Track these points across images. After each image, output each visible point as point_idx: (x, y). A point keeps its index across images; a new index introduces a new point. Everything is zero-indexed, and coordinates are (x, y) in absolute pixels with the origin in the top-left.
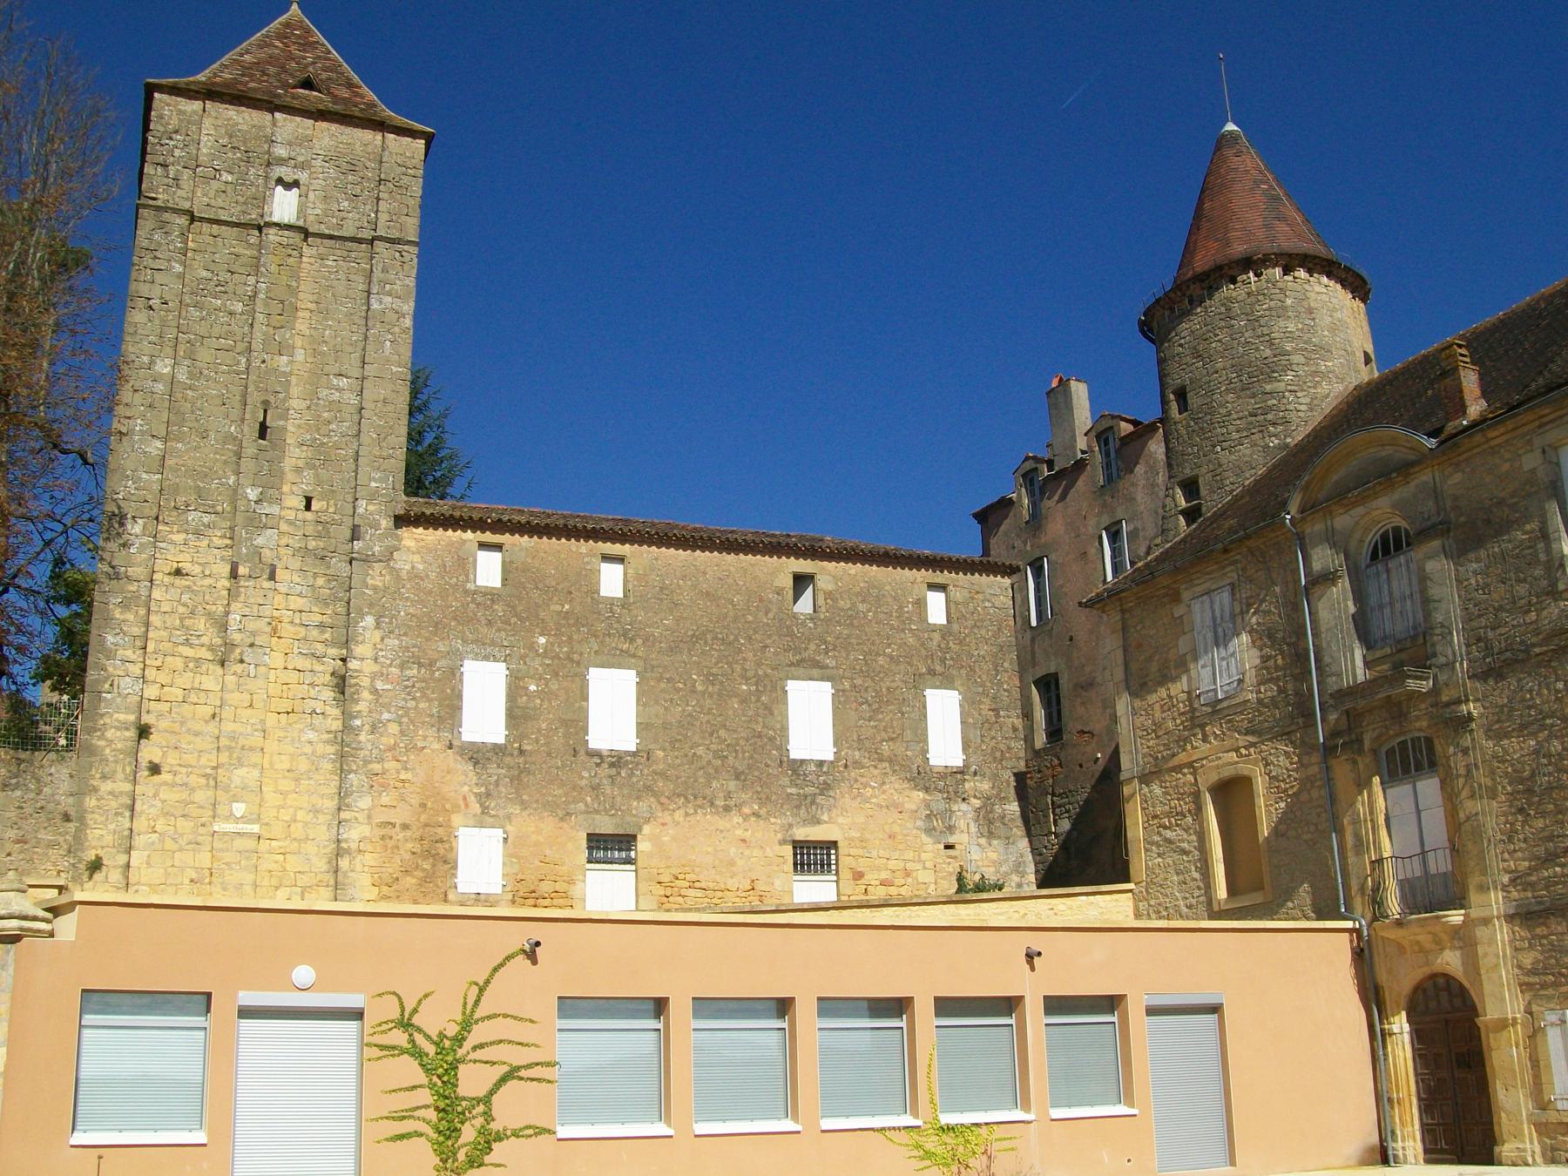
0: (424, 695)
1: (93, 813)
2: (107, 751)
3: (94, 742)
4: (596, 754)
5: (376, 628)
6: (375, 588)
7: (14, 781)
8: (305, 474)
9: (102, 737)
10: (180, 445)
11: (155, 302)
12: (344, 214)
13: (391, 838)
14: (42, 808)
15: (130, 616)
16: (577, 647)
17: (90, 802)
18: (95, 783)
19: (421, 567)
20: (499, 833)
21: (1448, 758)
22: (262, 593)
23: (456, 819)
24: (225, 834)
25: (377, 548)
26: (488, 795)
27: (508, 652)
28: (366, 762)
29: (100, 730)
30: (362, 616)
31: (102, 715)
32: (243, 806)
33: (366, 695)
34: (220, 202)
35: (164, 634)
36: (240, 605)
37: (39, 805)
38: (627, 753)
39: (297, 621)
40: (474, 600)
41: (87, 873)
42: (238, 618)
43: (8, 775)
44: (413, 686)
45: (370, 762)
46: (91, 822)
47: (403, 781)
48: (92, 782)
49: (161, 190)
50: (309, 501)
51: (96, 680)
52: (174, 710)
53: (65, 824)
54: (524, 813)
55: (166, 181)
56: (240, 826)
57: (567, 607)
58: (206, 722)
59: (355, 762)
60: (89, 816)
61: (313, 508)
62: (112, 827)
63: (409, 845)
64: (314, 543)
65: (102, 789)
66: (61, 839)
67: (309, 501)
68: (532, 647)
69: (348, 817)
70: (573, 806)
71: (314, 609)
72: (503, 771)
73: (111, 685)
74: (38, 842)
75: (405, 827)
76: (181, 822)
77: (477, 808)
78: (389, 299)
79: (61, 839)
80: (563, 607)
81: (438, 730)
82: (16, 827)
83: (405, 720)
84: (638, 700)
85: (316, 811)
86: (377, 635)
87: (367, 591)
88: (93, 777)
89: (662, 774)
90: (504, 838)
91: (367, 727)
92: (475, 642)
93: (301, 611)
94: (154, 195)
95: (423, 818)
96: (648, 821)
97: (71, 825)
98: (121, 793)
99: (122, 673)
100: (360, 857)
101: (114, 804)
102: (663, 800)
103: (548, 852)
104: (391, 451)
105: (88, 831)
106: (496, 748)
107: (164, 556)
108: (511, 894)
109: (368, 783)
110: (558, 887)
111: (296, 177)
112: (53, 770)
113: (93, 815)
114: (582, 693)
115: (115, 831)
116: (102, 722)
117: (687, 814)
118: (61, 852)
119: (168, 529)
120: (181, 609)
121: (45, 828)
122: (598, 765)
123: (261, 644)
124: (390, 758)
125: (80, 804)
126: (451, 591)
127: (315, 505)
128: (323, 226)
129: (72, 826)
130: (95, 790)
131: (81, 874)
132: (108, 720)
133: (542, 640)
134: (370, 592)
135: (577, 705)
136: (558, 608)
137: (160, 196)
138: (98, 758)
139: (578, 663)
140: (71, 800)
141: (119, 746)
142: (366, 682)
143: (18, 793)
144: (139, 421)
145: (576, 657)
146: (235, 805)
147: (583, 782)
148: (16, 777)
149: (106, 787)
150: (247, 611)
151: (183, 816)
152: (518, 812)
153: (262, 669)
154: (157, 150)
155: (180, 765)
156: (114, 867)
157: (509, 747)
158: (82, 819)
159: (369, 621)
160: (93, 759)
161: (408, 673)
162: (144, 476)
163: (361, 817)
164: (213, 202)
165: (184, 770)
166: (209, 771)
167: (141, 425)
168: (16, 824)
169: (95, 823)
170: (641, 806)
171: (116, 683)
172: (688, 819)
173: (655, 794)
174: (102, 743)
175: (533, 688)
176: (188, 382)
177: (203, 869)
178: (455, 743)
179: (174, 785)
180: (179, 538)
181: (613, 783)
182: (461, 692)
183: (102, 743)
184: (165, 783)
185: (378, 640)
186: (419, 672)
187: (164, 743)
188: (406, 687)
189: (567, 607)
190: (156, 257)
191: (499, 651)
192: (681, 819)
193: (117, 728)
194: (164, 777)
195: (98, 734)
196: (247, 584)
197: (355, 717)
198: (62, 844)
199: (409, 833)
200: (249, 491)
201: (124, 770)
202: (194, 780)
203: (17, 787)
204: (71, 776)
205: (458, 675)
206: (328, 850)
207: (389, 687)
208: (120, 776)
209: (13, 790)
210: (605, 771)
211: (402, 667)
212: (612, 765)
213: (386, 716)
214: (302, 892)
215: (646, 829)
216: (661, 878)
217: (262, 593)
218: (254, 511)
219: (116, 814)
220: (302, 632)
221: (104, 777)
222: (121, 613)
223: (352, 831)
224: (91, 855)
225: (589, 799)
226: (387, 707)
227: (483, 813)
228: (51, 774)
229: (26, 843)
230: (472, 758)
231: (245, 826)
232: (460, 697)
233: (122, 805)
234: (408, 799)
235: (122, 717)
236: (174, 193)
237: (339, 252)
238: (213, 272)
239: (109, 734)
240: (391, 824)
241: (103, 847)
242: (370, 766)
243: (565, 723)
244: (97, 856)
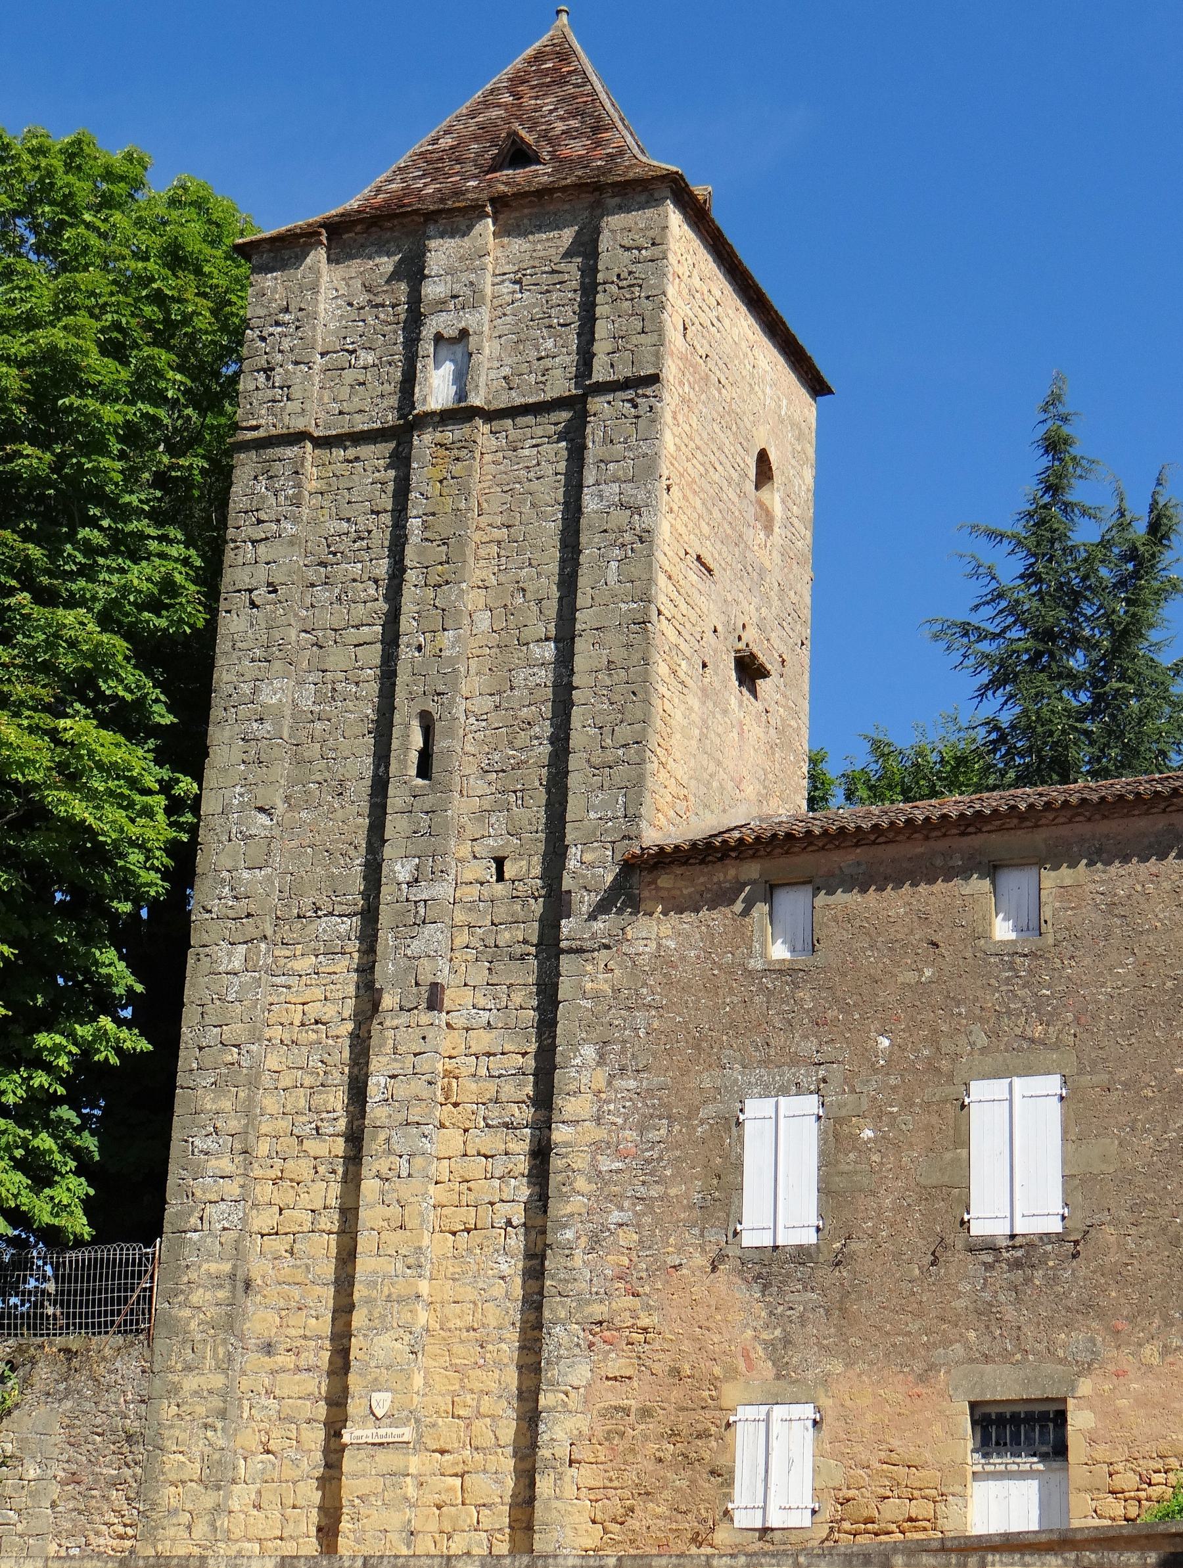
0: (678, 1173)
1: (171, 1427)
2: (193, 1325)
3: (174, 1312)
4: (989, 1246)
5: (599, 1064)
6: (597, 997)
7: (62, 1386)
8: (493, 820)
9: (186, 1304)
10: (304, 814)
11: (260, 594)
12: (548, 363)
13: (622, 1435)
15: (226, 1104)
16: (947, 1046)
19: (672, 944)
20: (808, 1411)
21: (158, 1556)
22: (419, 1032)
23: (730, 1393)
26: (787, 1341)
27: (821, 1073)
28: (582, 1302)
29: (182, 1292)
30: (575, 1047)
32: (388, 1396)
33: (581, 1183)
34: (356, 403)
35: (284, 1124)
36: (385, 1060)
38: (1046, 1237)
39: (484, 1072)
40: (763, 989)
42: (382, 1080)
44: (661, 1159)
45: (588, 1302)
49: (263, 412)
50: (500, 862)
54: (850, 1373)
55: (269, 394)
57: (928, 973)
59: (563, 1304)
61: (507, 876)
63: (652, 1447)
64: (507, 935)
67: (500, 862)
68: (867, 1053)
70: (941, 1350)
71: (507, 1048)
72: (814, 1296)
74: (96, 1481)
77: (767, 1369)
78: (615, 487)
80: (920, 972)
83: (647, 1220)
84: (1065, 1131)
86: (600, 1078)
87: (583, 1003)
89: (1117, 1275)
90: (815, 1423)
91: (583, 1241)
93: (489, 1055)
94: (254, 423)
95: (676, 1395)
96: (1086, 1369)
99: (214, 1198)
100: (573, 1471)
101: (201, 1410)
102: (1122, 1325)
103: (895, 1443)
104: (620, 752)
106: (802, 1254)
107: (282, 999)
108: (826, 1526)
109: (585, 1339)
110: (914, 1509)
111: (462, 325)
114: (956, 1129)
117: (1166, 1350)
119: (288, 953)
120: (308, 1081)
122: (988, 1267)
123: (417, 1119)
126: (723, 977)
127: (509, 870)
128: (513, 393)
132: (193, 1275)
133: (885, 1042)
134: (588, 1004)
135: (948, 1156)
136: (910, 977)
137: (262, 422)
139: (950, 1077)
142: (580, 1162)
144: (238, 789)
145: (945, 1065)
146: (376, 1396)
147: (960, 1304)
149: (190, 1383)
150: (396, 1068)
152: (840, 1369)
153: (418, 1161)
154: (257, 349)
155: (305, 1337)
157: (824, 1249)
159: (589, 1052)
161: (653, 1135)
162: (246, 875)
163: (574, 1400)
164: (346, 407)
167: (241, 795)
170: (1070, 1341)
172: (1170, 1359)
173: (1101, 1316)
175: (868, 1134)
176: (316, 709)
178: (732, 1251)
180: (304, 964)
181: (1018, 1300)
182: (740, 1157)
183: (186, 1313)
185: (602, 1084)
187: (282, 1304)
188: (648, 1161)
189: (928, 973)
190: (259, 522)
191: (807, 1075)
192: (1156, 1361)
196: (395, 1022)
197: (565, 1226)
199: (651, 1426)
200: (398, 868)
201: (215, 1350)
203: (68, 1393)
207: (620, 1165)
208: (209, 1362)
209: (60, 1400)
210: (1002, 1275)
211: (642, 1129)
212: (1017, 1264)
213: (616, 1216)
215: (1085, 1387)
216: (1118, 1482)
217: (419, 1032)
218: (408, 900)
220: (491, 1087)
222: (213, 1101)
225: (972, 1335)
226: (615, 1199)
227: (778, 1377)
231: (389, 1430)
235: (213, 1267)
236: (283, 409)
237: (539, 431)
238: (348, 520)
240: (623, 1409)
242: (588, 1310)
243: (928, 1194)
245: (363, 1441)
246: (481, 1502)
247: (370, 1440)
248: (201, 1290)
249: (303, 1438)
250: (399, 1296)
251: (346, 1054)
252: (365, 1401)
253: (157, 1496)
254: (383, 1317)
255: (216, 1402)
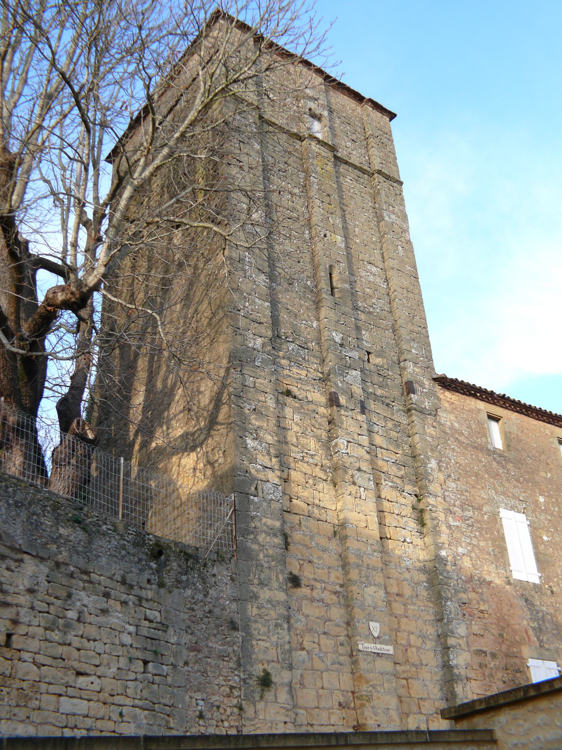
1: (256, 622)
2: (261, 556)
3: (249, 544)
7: (184, 578)
14: (210, 612)
17: (252, 611)
18: (255, 590)
23: (526, 651)
24: (368, 654)
25: (427, 404)
29: (252, 533)
31: (253, 518)
37: (207, 608)
41: (259, 689)
43: (179, 570)
46: (256, 633)
47: (482, 612)
48: (251, 587)
51: (243, 481)
52: (303, 523)
53: (232, 632)
56: (379, 646)
58: (329, 539)
60: (254, 625)
62: (274, 639)
63: (500, 675)
65: (262, 596)
66: (230, 650)
69: (454, 644)
73: (256, 489)
75: (494, 656)
76: (324, 640)
79: (230, 650)
81: (497, 566)
82: (190, 631)
85: (423, 637)
88: (251, 583)
92: (503, 493)
97: (236, 634)
98: (278, 602)
105: (254, 643)
112: (215, 571)
113: (257, 625)
115: (277, 644)
116: (253, 525)
118: (231, 665)
121: (215, 635)
124: (470, 589)
125: (242, 611)
129: (239, 635)
130: (255, 597)
131: (253, 691)
138: (254, 562)
140: (234, 606)
141: (271, 552)
143: (189, 592)
148: (186, 574)
149: (265, 594)
151: (325, 633)
156: (282, 684)
158: (247, 628)
160: (250, 563)
163: (462, 642)
165: (318, 585)
166: (338, 588)
168: (189, 627)
169: (259, 634)
171: (259, 487)
174: (255, 547)
177: (347, 691)
179: (312, 600)
182: (503, 534)
184: (305, 597)
186: (474, 514)
193: (268, 534)
194: (304, 591)
195: (252, 536)
196: (346, 414)
198: (232, 655)
202: (327, 596)
204: (232, 580)
205: (499, 520)
206: (438, 678)
208: (275, 584)
209: (184, 588)
214: (427, 721)
219: (277, 625)
221: (261, 584)
223: (460, 658)
224: (258, 670)
228: (214, 575)
229: (199, 651)
230: (522, 595)
231: (383, 646)
232: (503, 539)
233: (279, 615)
234: (490, 629)
235: (269, 522)
239: (261, 538)
241: (269, 662)
244: (265, 671)
245: (370, 650)
246: (420, 697)
247: (373, 651)
248: (264, 535)
249: (321, 643)
250: (373, 566)
251: (131, 411)
252: (365, 626)
253: (252, 669)
254: (367, 577)
255: (282, 611)
